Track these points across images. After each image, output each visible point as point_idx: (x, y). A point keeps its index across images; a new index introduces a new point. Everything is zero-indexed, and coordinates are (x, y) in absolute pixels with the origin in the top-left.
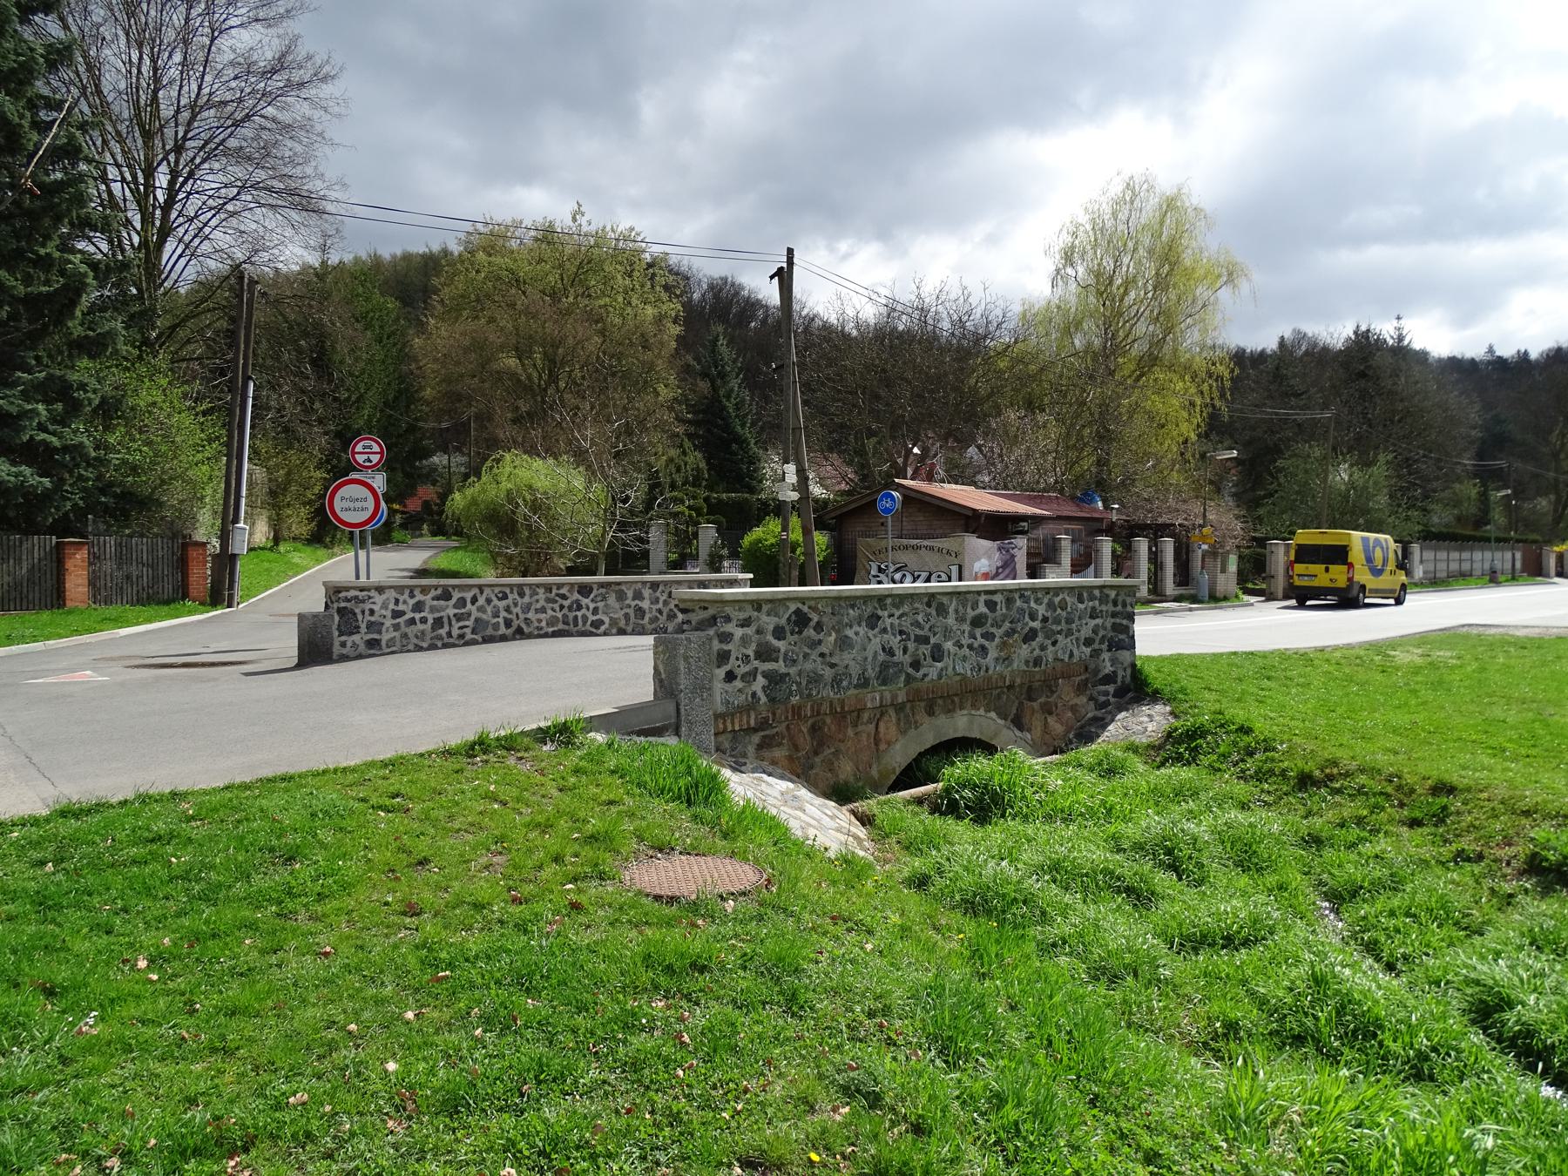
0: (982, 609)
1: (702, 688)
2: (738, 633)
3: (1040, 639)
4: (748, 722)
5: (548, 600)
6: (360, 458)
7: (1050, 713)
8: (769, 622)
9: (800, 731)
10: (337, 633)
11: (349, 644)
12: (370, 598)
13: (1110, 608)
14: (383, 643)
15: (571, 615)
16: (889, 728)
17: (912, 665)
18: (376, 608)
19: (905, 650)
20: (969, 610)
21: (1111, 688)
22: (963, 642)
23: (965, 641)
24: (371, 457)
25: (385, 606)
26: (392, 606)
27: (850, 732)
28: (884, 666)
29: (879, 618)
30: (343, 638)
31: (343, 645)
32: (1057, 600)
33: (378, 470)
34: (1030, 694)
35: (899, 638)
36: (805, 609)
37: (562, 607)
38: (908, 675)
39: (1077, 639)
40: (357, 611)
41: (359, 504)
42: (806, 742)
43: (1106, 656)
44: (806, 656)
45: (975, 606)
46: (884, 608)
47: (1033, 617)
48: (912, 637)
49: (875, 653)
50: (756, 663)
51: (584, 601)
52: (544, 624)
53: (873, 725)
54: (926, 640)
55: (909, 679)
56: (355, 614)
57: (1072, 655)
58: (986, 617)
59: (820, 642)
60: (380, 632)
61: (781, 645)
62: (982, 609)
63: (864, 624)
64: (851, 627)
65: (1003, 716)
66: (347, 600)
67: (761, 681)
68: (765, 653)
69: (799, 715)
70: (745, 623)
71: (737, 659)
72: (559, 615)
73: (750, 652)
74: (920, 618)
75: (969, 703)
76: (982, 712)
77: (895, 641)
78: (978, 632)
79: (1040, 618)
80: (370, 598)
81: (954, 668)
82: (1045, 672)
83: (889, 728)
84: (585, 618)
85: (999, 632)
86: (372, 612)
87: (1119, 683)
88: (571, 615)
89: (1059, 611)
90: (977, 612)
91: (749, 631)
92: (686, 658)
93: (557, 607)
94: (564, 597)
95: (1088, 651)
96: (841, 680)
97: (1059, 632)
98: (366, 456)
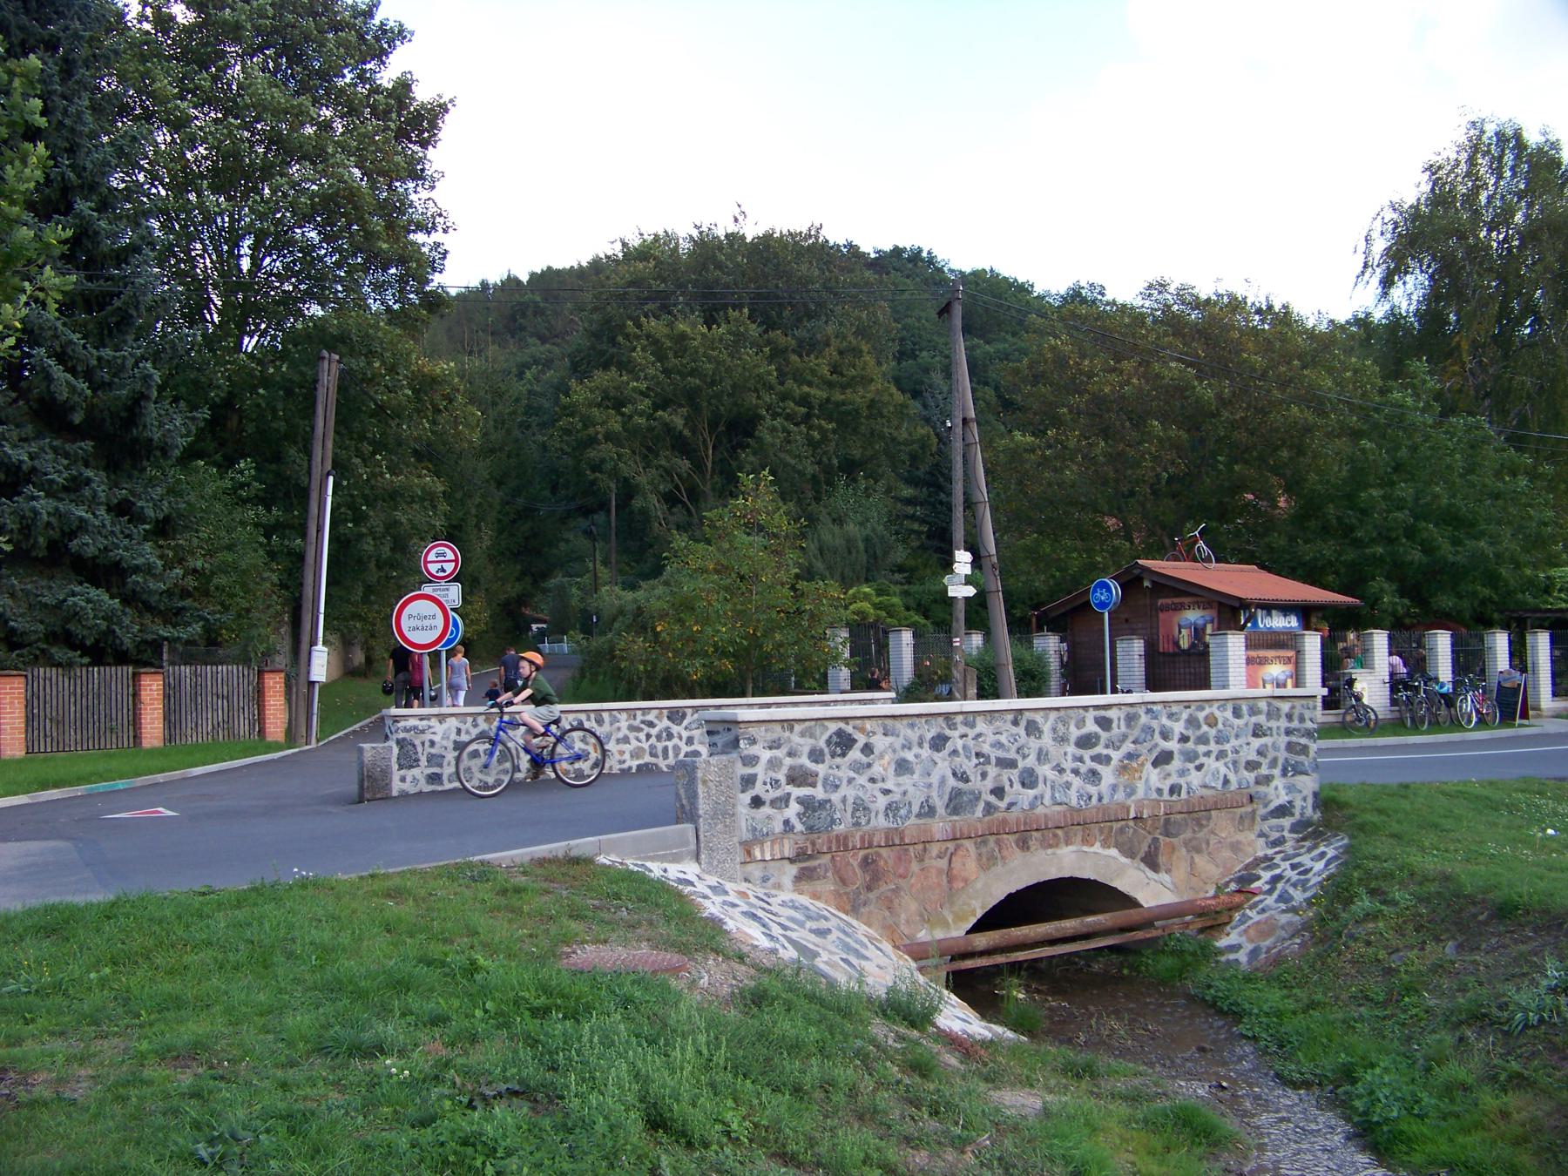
0: (1091, 727)
1: (725, 813)
2: (766, 755)
3: (1177, 763)
4: (782, 851)
5: (632, 728)
6: (433, 568)
7: (1198, 850)
8: (805, 744)
9: (848, 863)
10: (395, 767)
11: (409, 779)
12: (430, 727)
13: (1283, 723)
14: (445, 778)
15: (660, 746)
16: (967, 861)
17: (993, 792)
18: (437, 738)
19: (984, 775)
20: (1072, 728)
21: (1286, 822)
22: (1065, 765)
23: (1068, 765)
24: (445, 565)
25: (445, 737)
26: (453, 736)
27: (915, 867)
28: (956, 795)
29: (946, 739)
30: (402, 772)
31: (403, 779)
32: (1201, 715)
33: (454, 580)
34: (1168, 829)
35: (975, 761)
36: (849, 729)
37: (648, 736)
38: (988, 804)
39: (1235, 763)
40: (417, 742)
41: (427, 623)
42: (860, 878)
43: (1278, 782)
44: (850, 781)
45: (1081, 723)
46: (952, 726)
47: (1165, 735)
48: (993, 761)
49: (943, 781)
50: (789, 788)
51: (675, 729)
52: (627, 756)
53: (945, 861)
54: (1012, 764)
55: (989, 808)
56: (414, 746)
57: (1226, 781)
58: (1097, 737)
59: (869, 765)
60: (441, 766)
61: (821, 769)
62: (1091, 727)
63: (926, 745)
64: (910, 749)
65: (1129, 853)
66: (406, 730)
67: (793, 809)
68: (799, 777)
69: (846, 846)
70: (774, 745)
71: (765, 783)
72: (646, 746)
73: (781, 776)
74: (1003, 739)
75: (1079, 838)
76: (1097, 848)
77: (969, 765)
78: (1087, 754)
79: (1176, 737)
80: (430, 727)
81: (1053, 797)
82: (1187, 801)
83: (967, 861)
84: (677, 749)
85: (1116, 756)
86: (432, 743)
87: (1297, 816)
88: (660, 746)
89: (1205, 728)
90: (1085, 731)
91: (779, 753)
92: (705, 782)
93: (642, 736)
94: (651, 724)
95: (1251, 776)
96: (898, 809)
97: (1208, 754)
98: (438, 566)
